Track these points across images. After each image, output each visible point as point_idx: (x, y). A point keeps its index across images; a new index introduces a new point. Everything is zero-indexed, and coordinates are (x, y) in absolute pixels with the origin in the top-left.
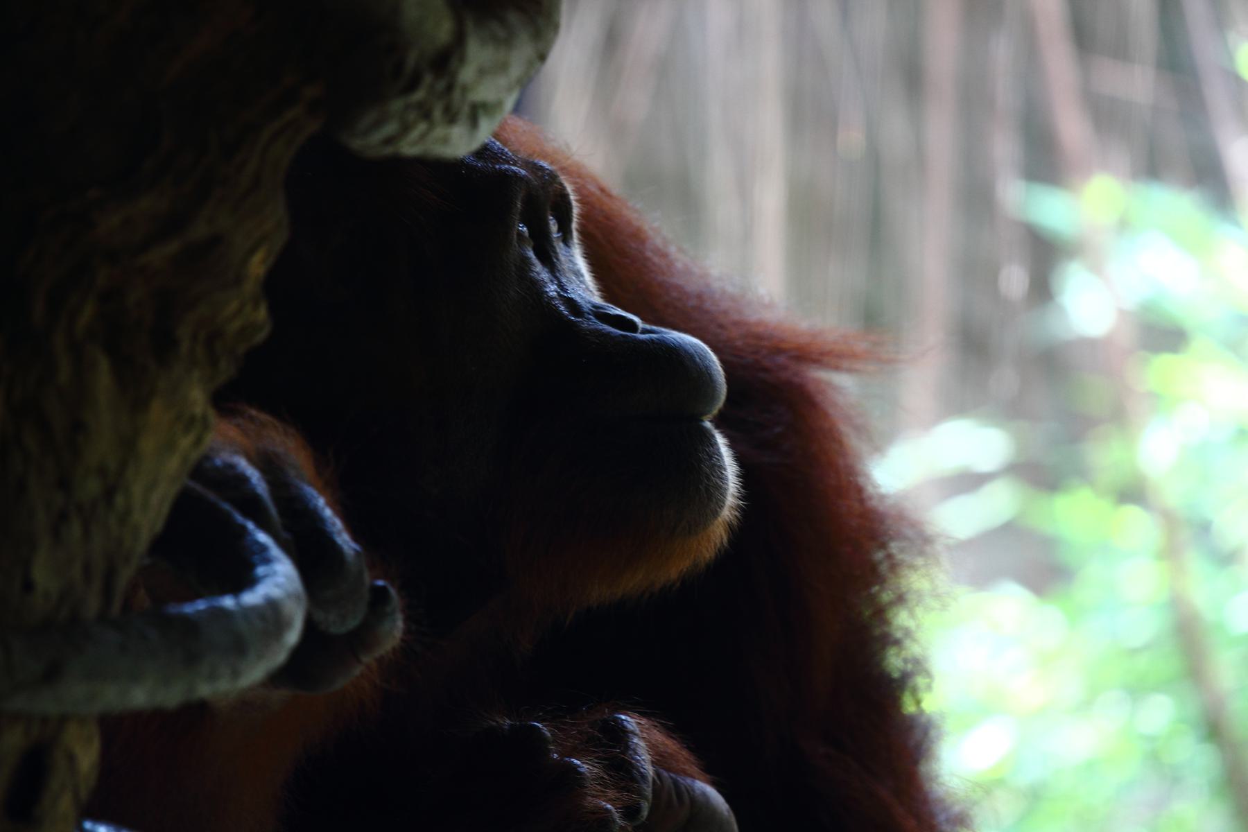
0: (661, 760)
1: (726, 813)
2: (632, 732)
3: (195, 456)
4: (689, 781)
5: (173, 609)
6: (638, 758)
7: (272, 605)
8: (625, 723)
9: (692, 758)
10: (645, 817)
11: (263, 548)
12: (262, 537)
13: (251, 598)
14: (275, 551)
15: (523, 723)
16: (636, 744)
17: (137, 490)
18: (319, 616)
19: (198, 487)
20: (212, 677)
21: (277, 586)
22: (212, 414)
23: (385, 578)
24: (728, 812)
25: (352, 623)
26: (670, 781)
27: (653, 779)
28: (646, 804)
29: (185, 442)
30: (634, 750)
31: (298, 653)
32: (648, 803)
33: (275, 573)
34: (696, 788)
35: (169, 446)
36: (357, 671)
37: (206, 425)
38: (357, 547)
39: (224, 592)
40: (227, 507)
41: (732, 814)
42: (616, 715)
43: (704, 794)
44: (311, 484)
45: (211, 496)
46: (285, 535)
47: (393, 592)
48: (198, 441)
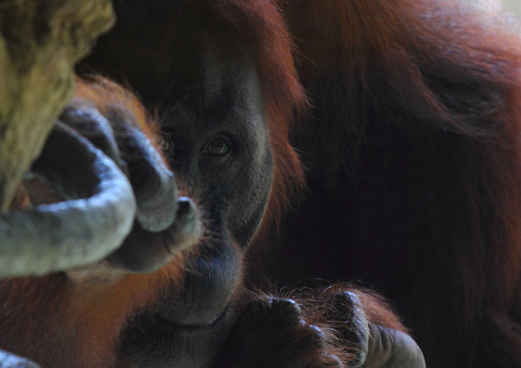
0: (375, 320)
1: (417, 353)
2: (356, 305)
3: (61, 106)
4: (392, 332)
5: (44, 208)
6: (360, 322)
7: (111, 208)
8: (352, 298)
9: (295, 72)
10: (363, 363)
11: (107, 169)
12: (107, 162)
13: (97, 202)
14: (115, 171)
15: (282, 299)
16: (359, 313)
17: (21, 128)
18: (143, 219)
19: (66, 127)
20: (69, 254)
21: (115, 194)
22: (73, 76)
23: (190, 195)
24: (418, 352)
25: (165, 225)
26: (379, 332)
27: (369, 337)
28: (364, 354)
29: (55, 96)
30: (357, 317)
31: (128, 240)
32: (365, 353)
33: (114, 186)
34: (396, 337)
35: (44, 99)
36: (169, 259)
37: (69, 86)
38: (171, 174)
39: (80, 197)
40: (84, 140)
41: (421, 353)
42: (345, 292)
43: (402, 341)
44: (141, 130)
45: (74, 133)
46: (123, 163)
47: (193, 205)
48: (64, 96)
